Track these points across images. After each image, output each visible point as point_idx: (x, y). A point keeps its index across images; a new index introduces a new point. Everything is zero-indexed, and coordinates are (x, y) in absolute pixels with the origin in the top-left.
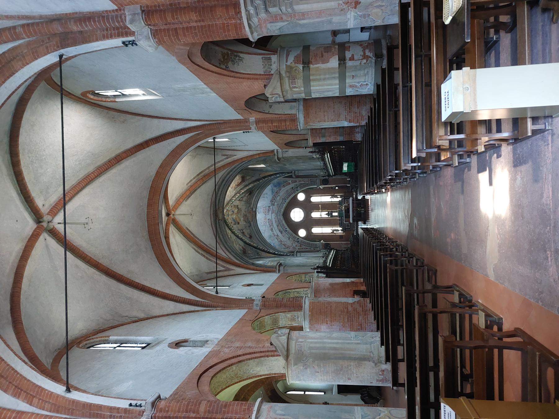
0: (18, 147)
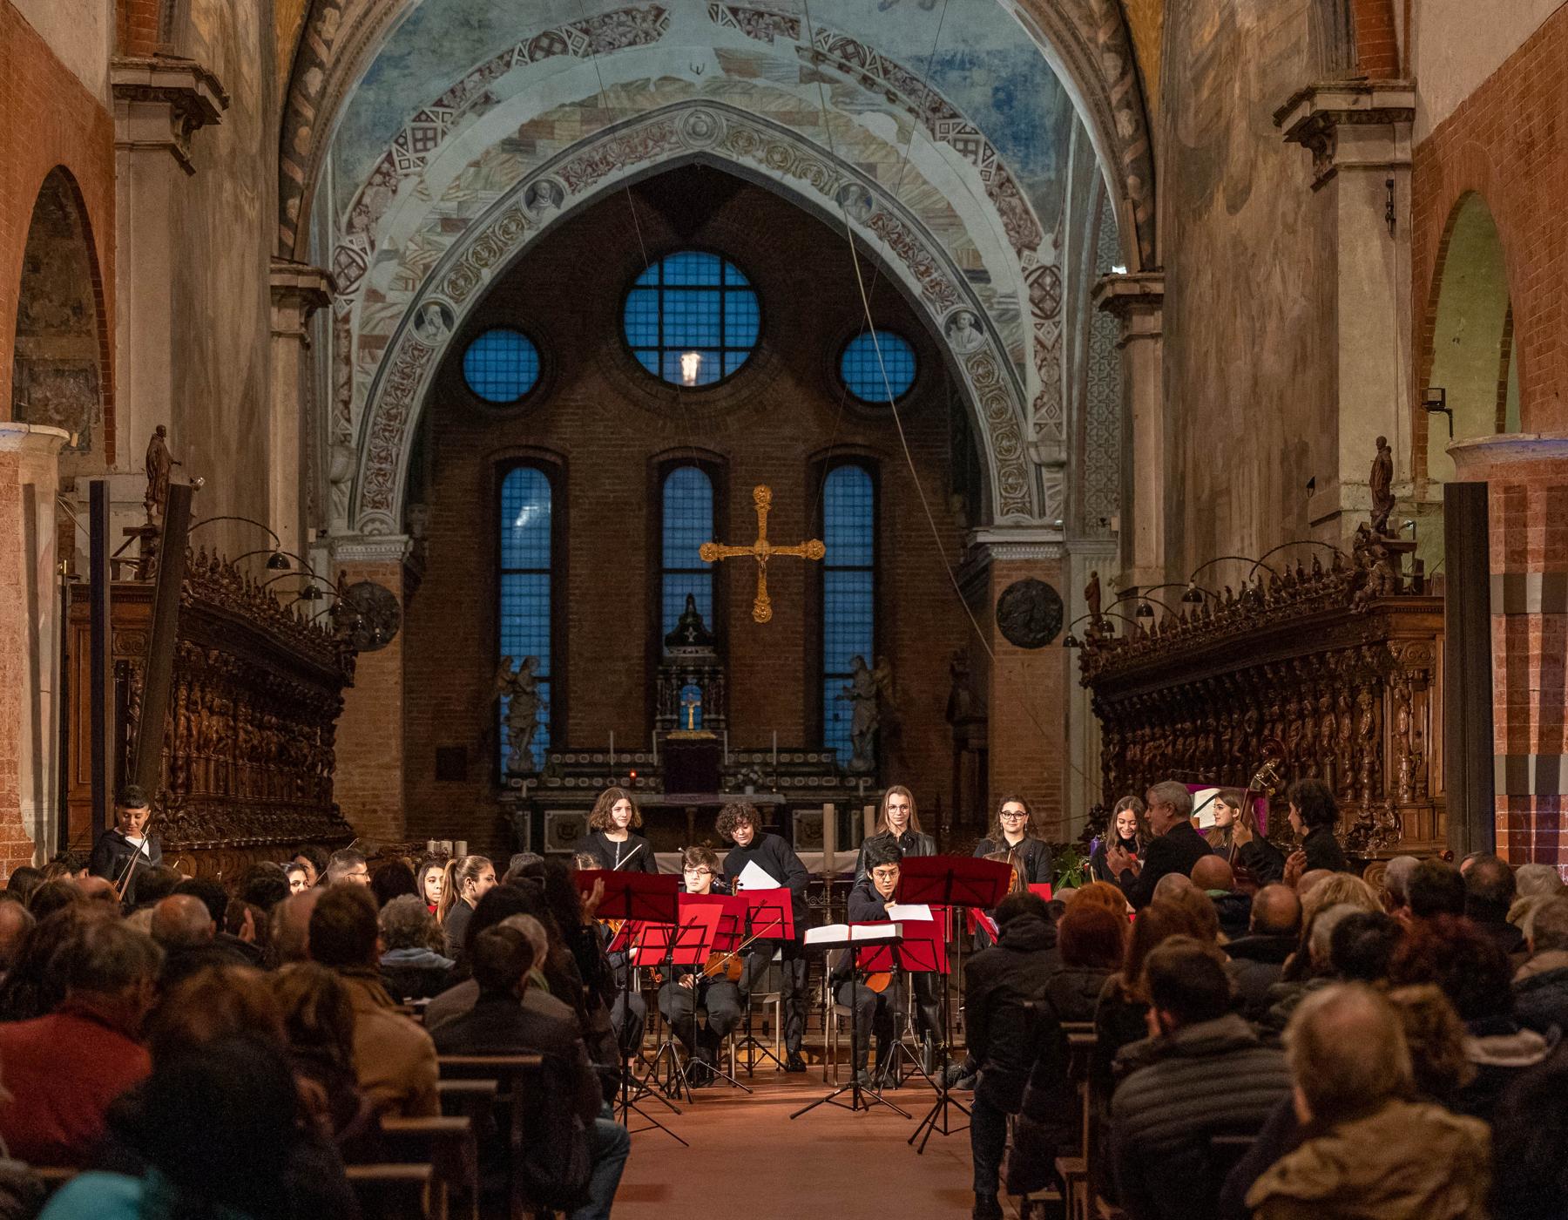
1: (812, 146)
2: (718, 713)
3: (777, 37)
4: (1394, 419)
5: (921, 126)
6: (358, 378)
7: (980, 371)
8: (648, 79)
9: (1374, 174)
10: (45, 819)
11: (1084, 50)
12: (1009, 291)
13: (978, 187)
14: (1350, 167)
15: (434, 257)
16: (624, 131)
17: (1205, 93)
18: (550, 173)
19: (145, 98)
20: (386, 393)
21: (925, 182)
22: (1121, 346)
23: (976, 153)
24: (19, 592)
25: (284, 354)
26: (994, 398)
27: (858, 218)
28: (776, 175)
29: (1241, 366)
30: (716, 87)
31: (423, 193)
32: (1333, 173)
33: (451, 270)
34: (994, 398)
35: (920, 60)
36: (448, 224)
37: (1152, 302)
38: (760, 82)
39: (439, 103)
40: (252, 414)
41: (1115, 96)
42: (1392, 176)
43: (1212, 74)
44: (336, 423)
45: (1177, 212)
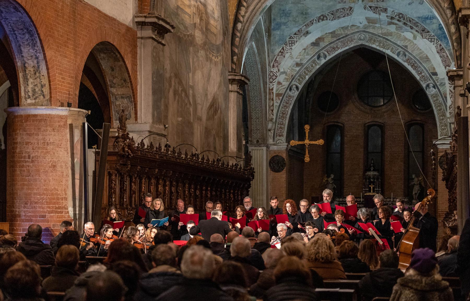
1: (391, 41)
2: (379, 188)
3: (382, 13)
5: (419, 35)
6: (275, 104)
7: (435, 99)
8: (348, 26)
10: (77, 213)
12: (442, 78)
13: (435, 51)
15: (294, 73)
16: (342, 39)
18: (323, 51)
19: (145, 25)
20: (282, 108)
21: (420, 50)
23: (434, 41)
25: (233, 97)
26: (438, 106)
27: (402, 60)
28: (381, 49)
30: (365, 27)
31: (291, 57)
33: (299, 76)
34: (438, 106)
35: (419, 18)
36: (298, 65)
37: (460, 77)
38: (377, 25)
39: (295, 34)
41: (450, 21)
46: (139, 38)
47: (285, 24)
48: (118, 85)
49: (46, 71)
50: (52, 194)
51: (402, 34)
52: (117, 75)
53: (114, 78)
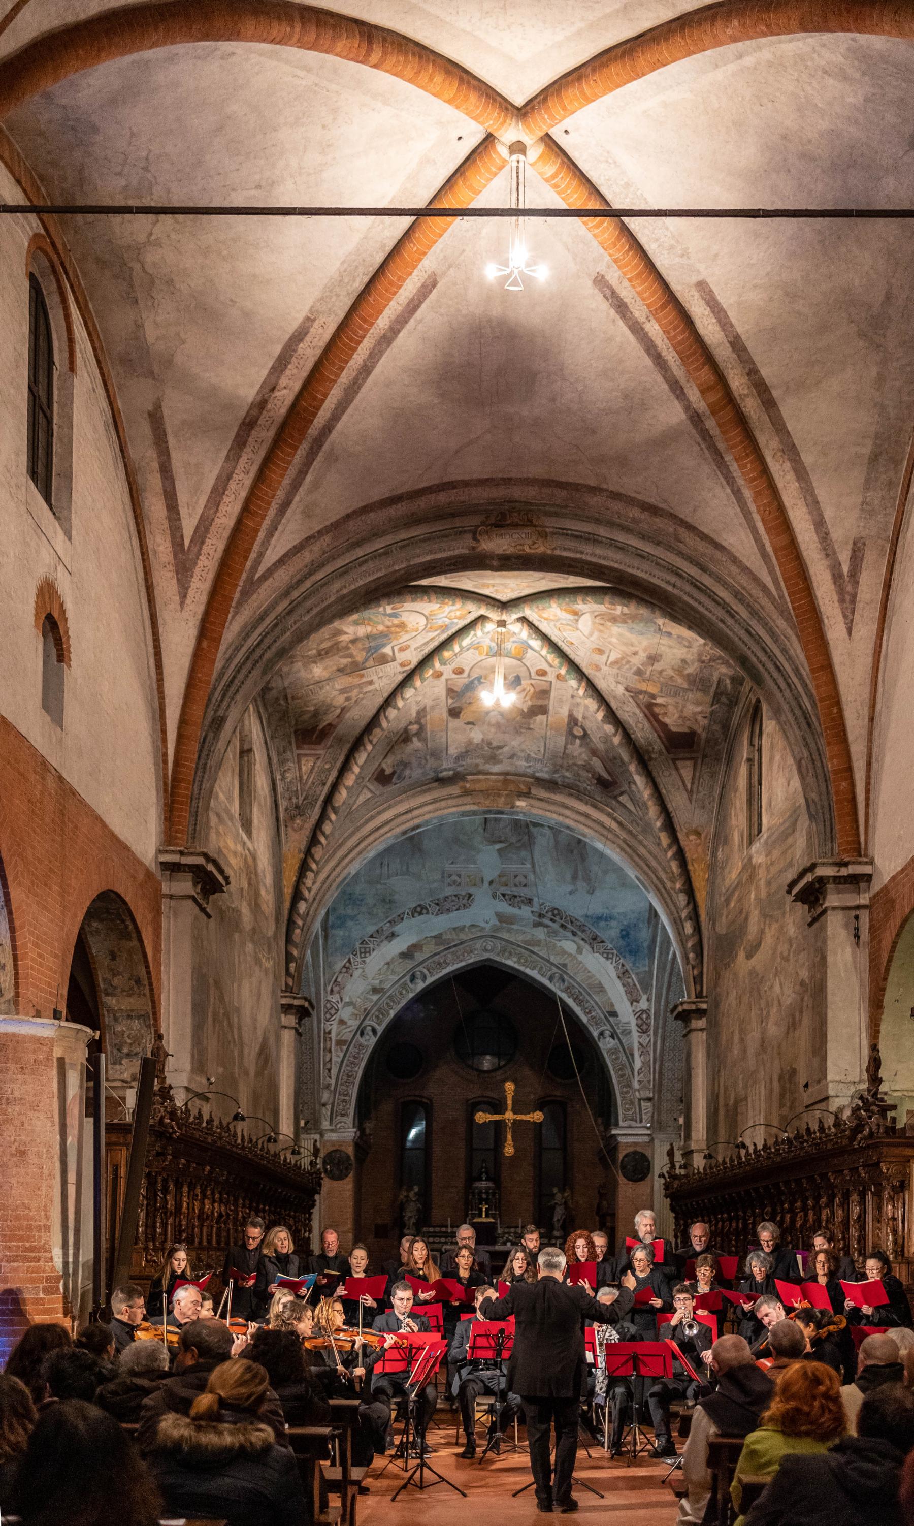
0: (805, 27)
4: (857, 1046)
5: (588, 947)
6: (334, 1059)
9: (848, 912)
10: (71, 1260)
11: (669, 893)
13: (613, 974)
14: (834, 908)
15: (368, 1005)
17: (732, 905)
18: (421, 968)
19: (179, 870)
22: (685, 1036)
24: (53, 1122)
25: (288, 1037)
28: (522, 968)
29: (753, 1037)
30: (496, 929)
31: (364, 976)
32: (824, 912)
35: (587, 916)
36: (375, 990)
37: (701, 1013)
38: (515, 927)
39: (371, 936)
40: (266, 1061)
41: (684, 915)
42: (858, 913)
43: (737, 894)
44: (325, 1078)
45: (715, 968)
46: (165, 896)
47: (353, 918)
48: (123, 991)
49: (8, 935)
50: (17, 1218)
51: (558, 944)
52: (121, 969)
53: (114, 975)
